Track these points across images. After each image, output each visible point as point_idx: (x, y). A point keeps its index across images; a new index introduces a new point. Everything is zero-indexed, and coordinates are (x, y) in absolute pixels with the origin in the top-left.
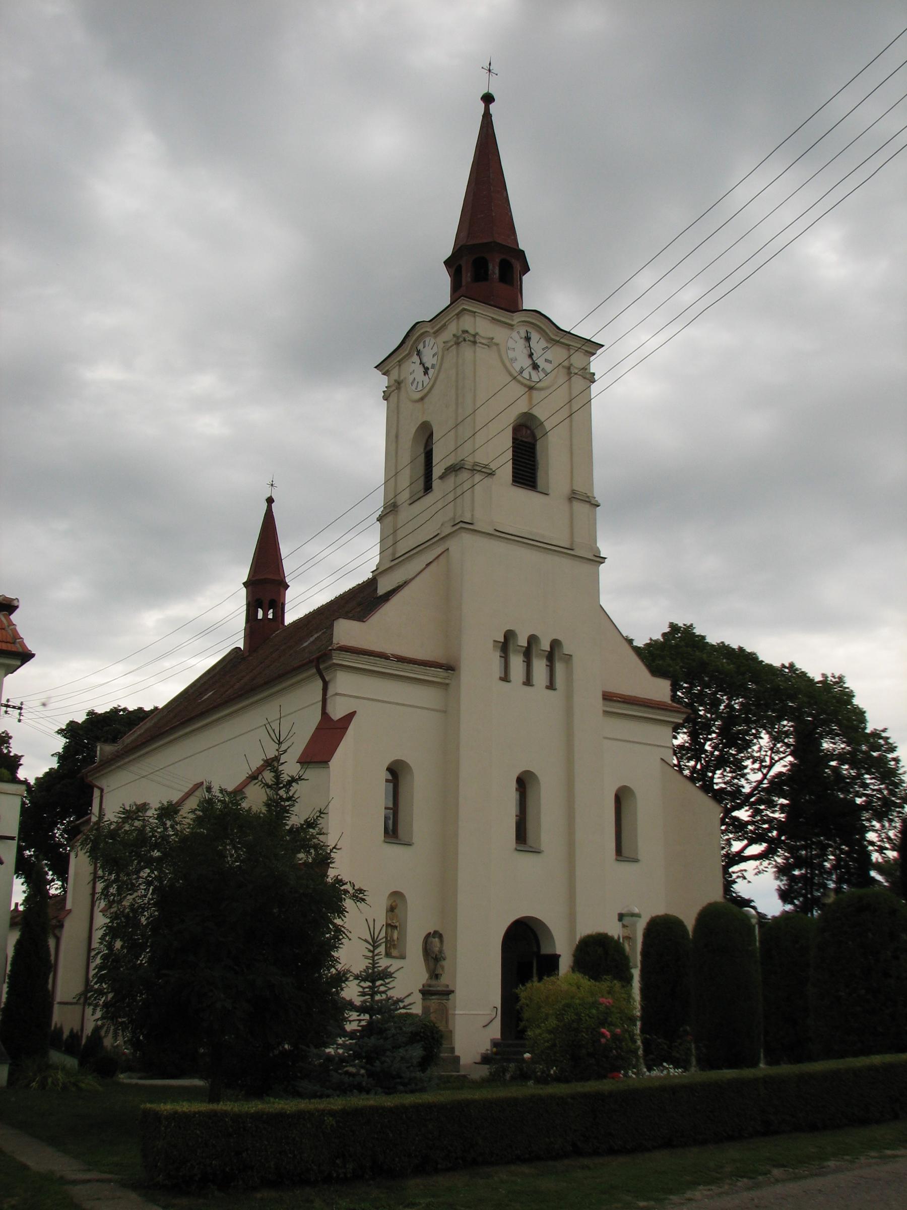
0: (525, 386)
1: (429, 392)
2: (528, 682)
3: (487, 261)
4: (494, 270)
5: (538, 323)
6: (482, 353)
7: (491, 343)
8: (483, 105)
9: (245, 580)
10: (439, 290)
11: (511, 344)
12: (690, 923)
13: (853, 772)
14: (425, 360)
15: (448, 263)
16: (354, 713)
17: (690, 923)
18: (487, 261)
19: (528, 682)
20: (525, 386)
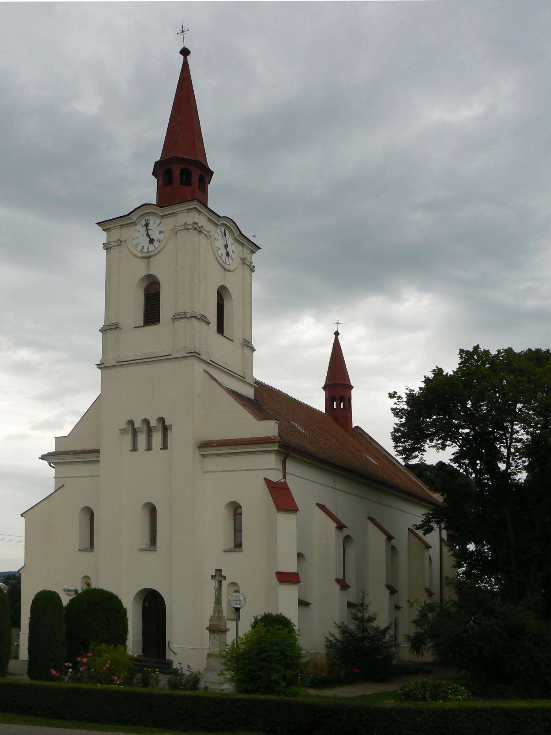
0: (144, 258)
1: (157, 254)
2: (149, 448)
3: (182, 171)
4: (195, 179)
5: (227, 224)
6: (203, 240)
7: (207, 236)
8: (183, 57)
9: (323, 386)
10: (148, 190)
11: (216, 236)
12: (65, 600)
13: (58, 675)
14: (150, 232)
15: (152, 174)
16: (317, 504)
17: (65, 600)
18: (182, 171)
19: (149, 448)
20: (144, 258)
